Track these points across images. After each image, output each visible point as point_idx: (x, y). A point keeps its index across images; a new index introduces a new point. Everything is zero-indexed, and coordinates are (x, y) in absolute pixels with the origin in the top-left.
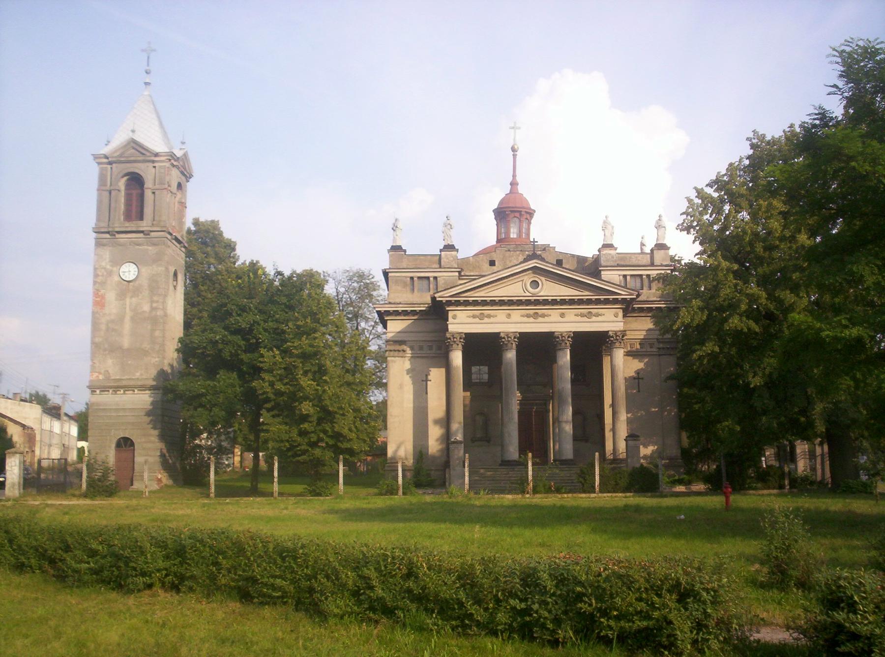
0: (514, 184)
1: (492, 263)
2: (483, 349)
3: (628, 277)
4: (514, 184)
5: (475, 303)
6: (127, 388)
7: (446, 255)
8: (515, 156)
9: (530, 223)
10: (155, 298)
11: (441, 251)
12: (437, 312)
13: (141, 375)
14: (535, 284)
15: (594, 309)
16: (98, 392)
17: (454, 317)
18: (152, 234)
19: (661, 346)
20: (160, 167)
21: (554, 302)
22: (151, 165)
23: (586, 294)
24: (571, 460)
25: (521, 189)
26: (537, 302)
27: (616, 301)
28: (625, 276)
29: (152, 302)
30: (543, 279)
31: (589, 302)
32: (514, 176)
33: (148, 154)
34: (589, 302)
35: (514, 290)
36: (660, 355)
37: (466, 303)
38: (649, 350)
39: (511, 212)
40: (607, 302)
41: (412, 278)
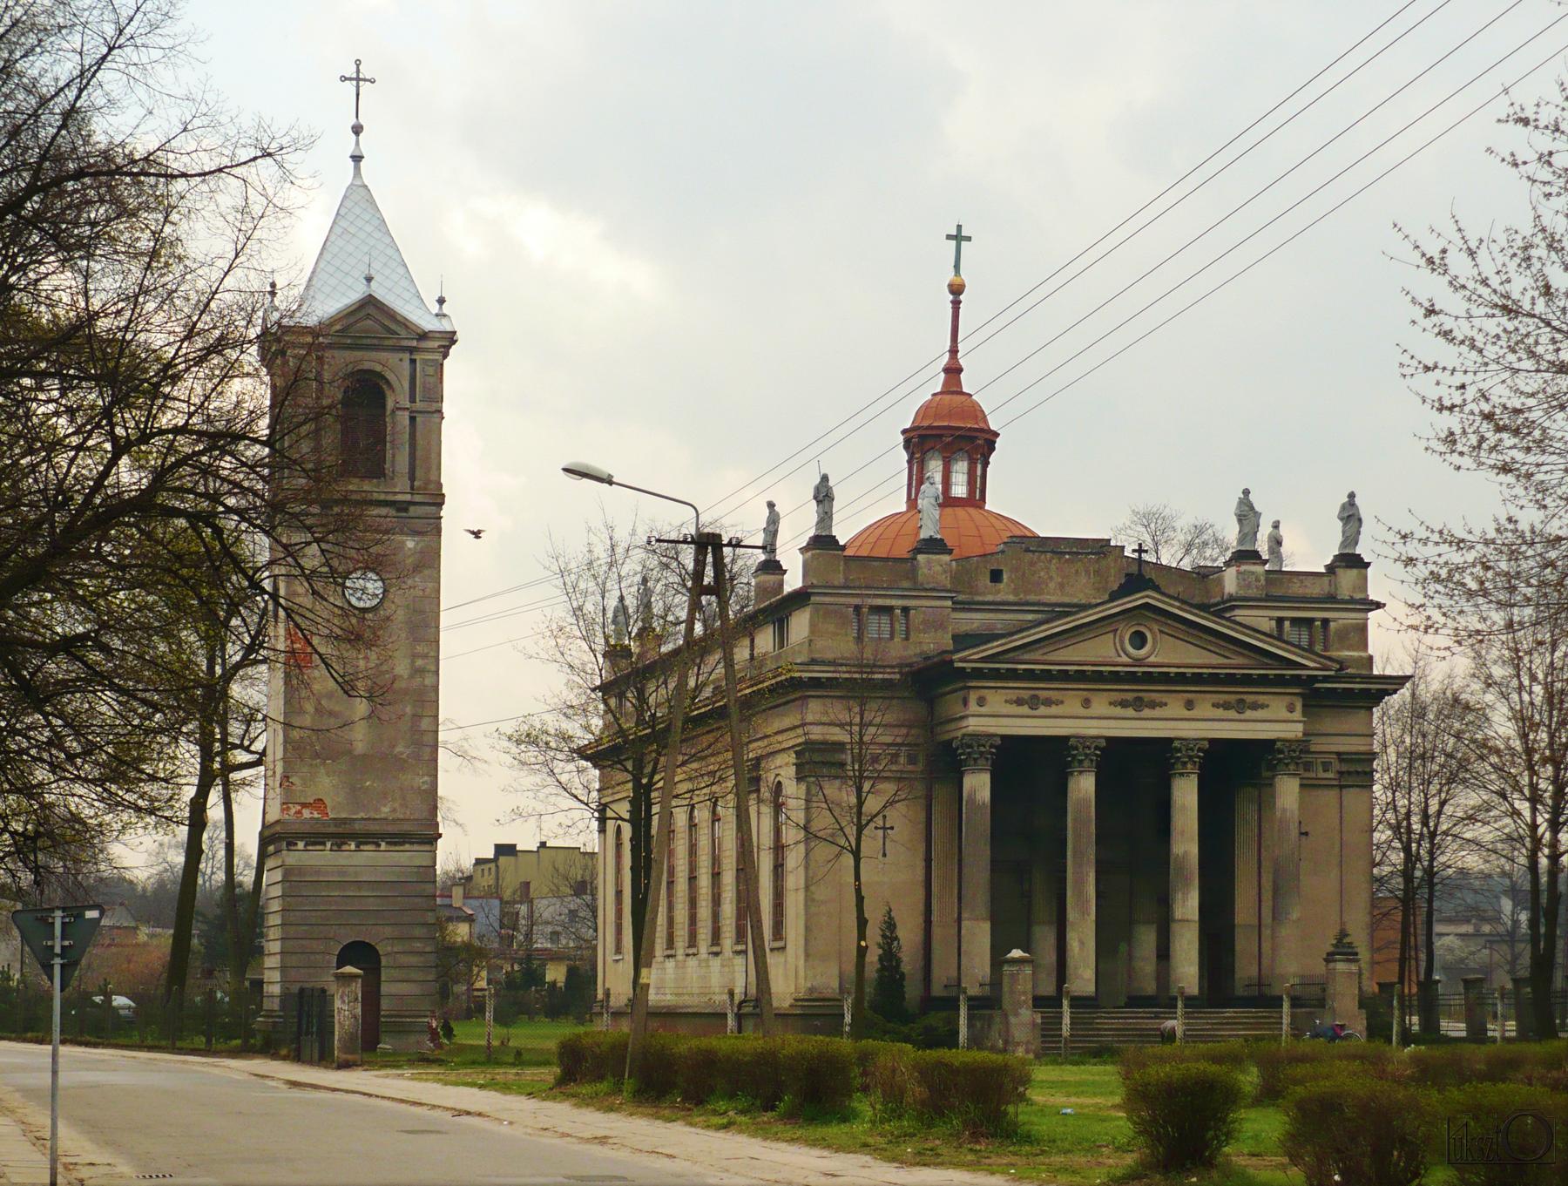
0: (953, 371)
1: (996, 576)
2: (1030, 768)
3: (1287, 624)
4: (953, 371)
5: (1030, 675)
6: (366, 838)
7: (929, 562)
8: (956, 304)
9: (986, 464)
10: (419, 649)
12: (933, 682)
13: (394, 810)
14: (1139, 640)
16: (301, 845)
17: (981, 702)
18: (412, 509)
19: (1344, 768)
20: (425, 361)
21: (1181, 679)
22: (406, 356)
23: (1235, 663)
24: (1150, 998)
25: (967, 383)
26: (1149, 678)
27: (1296, 681)
28: (1280, 621)
29: (414, 656)
30: (1156, 627)
31: (1247, 680)
32: (954, 351)
33: (403, 333)
34: (1247, 680)
35: (1104, 651)
36: (1341, 787)
37: (996, 675)
39: (951, 436)
40: (1280, 681)
41: (857, 608)
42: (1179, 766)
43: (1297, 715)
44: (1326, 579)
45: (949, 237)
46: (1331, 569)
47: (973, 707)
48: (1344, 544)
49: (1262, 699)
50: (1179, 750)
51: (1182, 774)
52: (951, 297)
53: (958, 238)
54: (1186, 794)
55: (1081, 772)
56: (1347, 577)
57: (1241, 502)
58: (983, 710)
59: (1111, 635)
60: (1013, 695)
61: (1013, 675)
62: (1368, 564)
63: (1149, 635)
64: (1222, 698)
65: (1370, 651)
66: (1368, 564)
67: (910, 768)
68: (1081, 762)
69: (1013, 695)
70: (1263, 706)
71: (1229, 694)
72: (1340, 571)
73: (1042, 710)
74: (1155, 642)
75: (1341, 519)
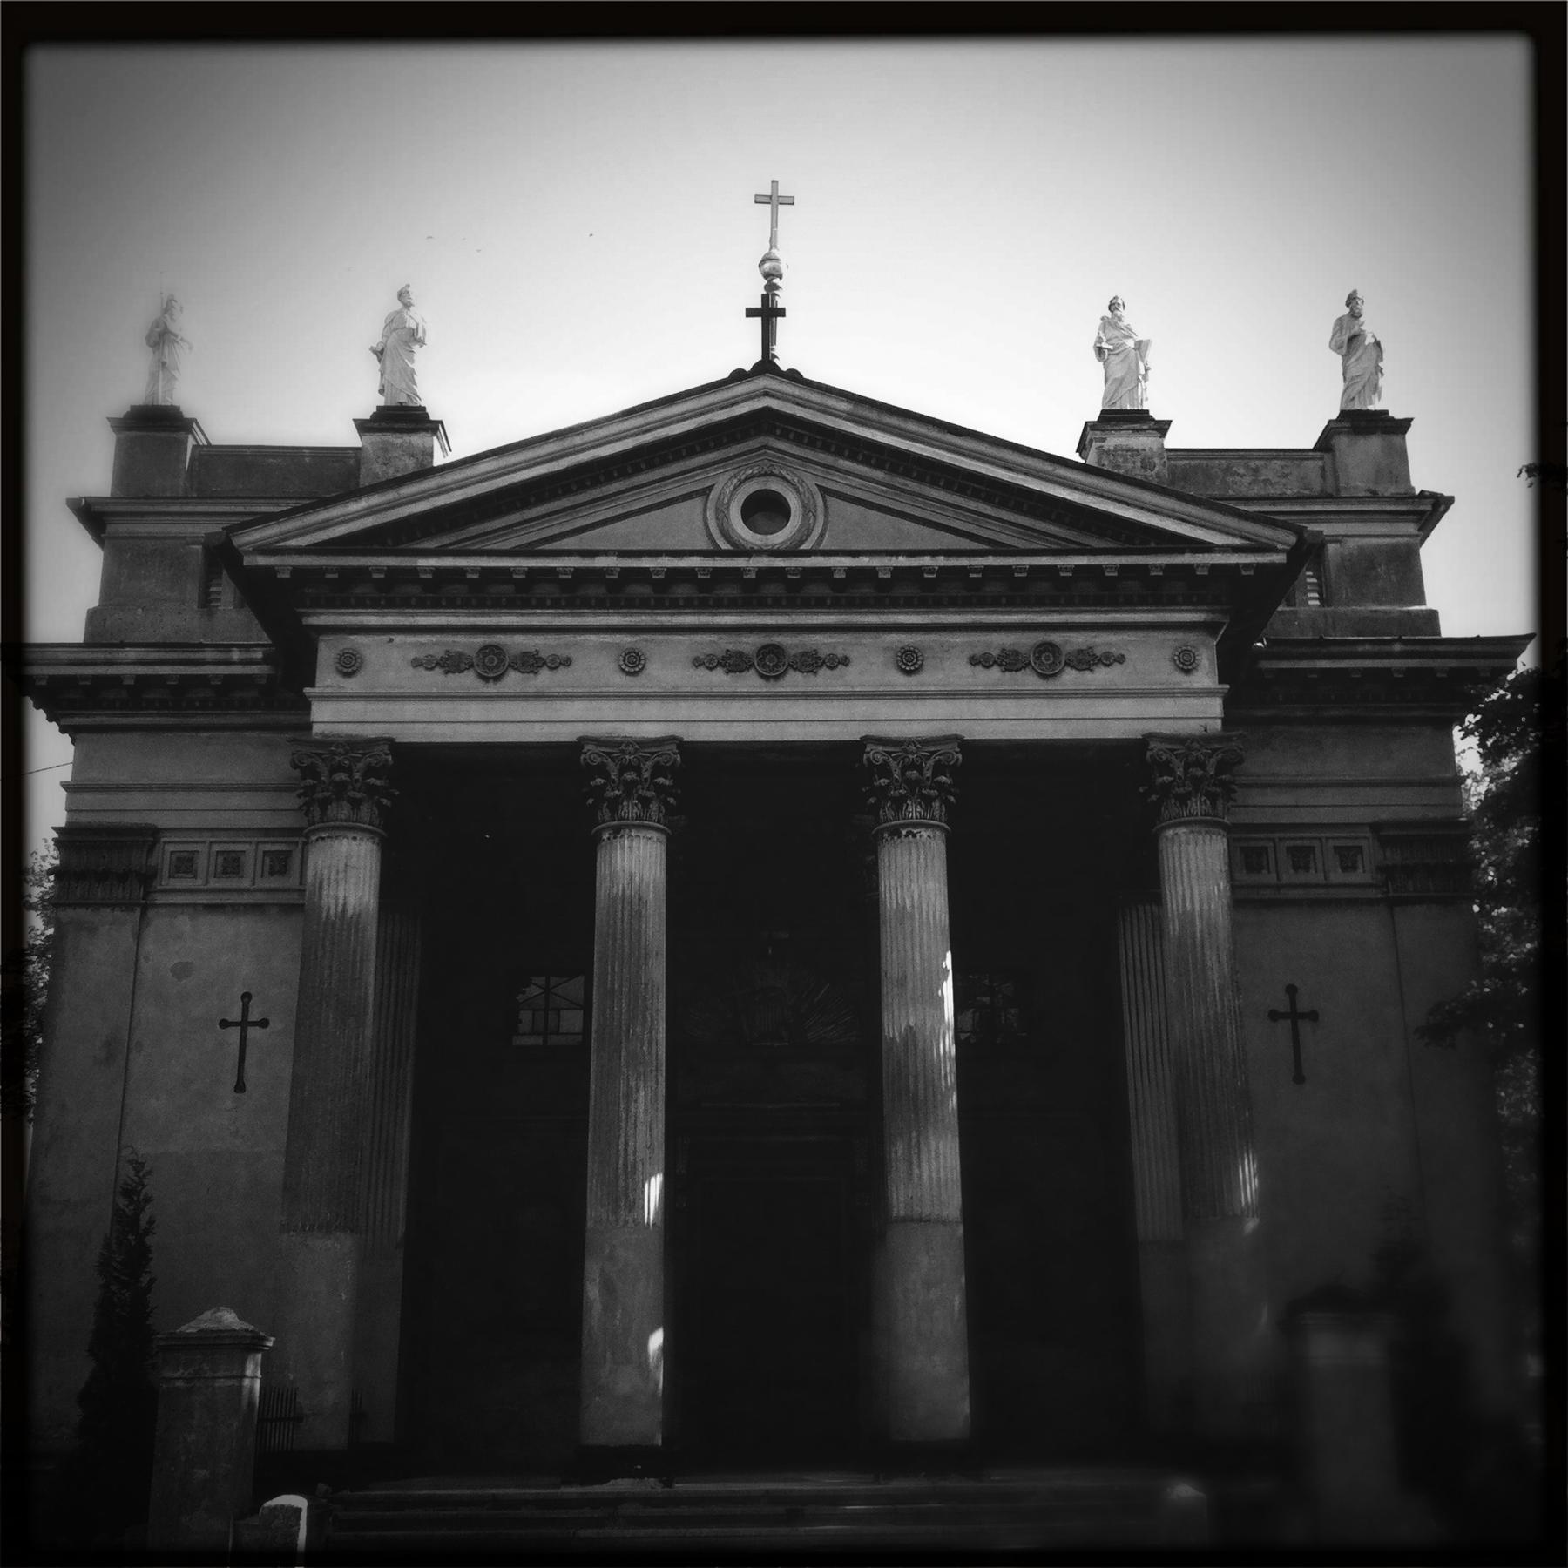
11: (363, 426)
15: (1075, 628)
17: (349, 665)
36: (1392, 903)
38: (1337, 876)
42: (887, 812)
43: (1205, 676)
44: (1313, 466)
45: (759, 200)
46: (1326, 443)
47: (326, 679)
48: (1347, 396)
49: (1102, 641)
50: (884, 770)
51: (895, 832)
52: (995, 653)
53: (773, 200)
54: (916, 883)
55: (617, 831)
56: (1360, 454)
57: (1106, 324)
58: (351, 685)
59: (697, 503)
60: (435, 645)
61: (441, 590)
62: (1405, 424)
63: (775, 486)
64: (998, 642)
65: (1431, 603)
66: (1405, 424)
67: (275, 882)
68: (614, 805)
69: (435, 645)
70: (1109, 660)
71: (1014, 627)
72: (1342, 442)
73: (513, 681)
74: (807, 510)
75: (1337, 347)
